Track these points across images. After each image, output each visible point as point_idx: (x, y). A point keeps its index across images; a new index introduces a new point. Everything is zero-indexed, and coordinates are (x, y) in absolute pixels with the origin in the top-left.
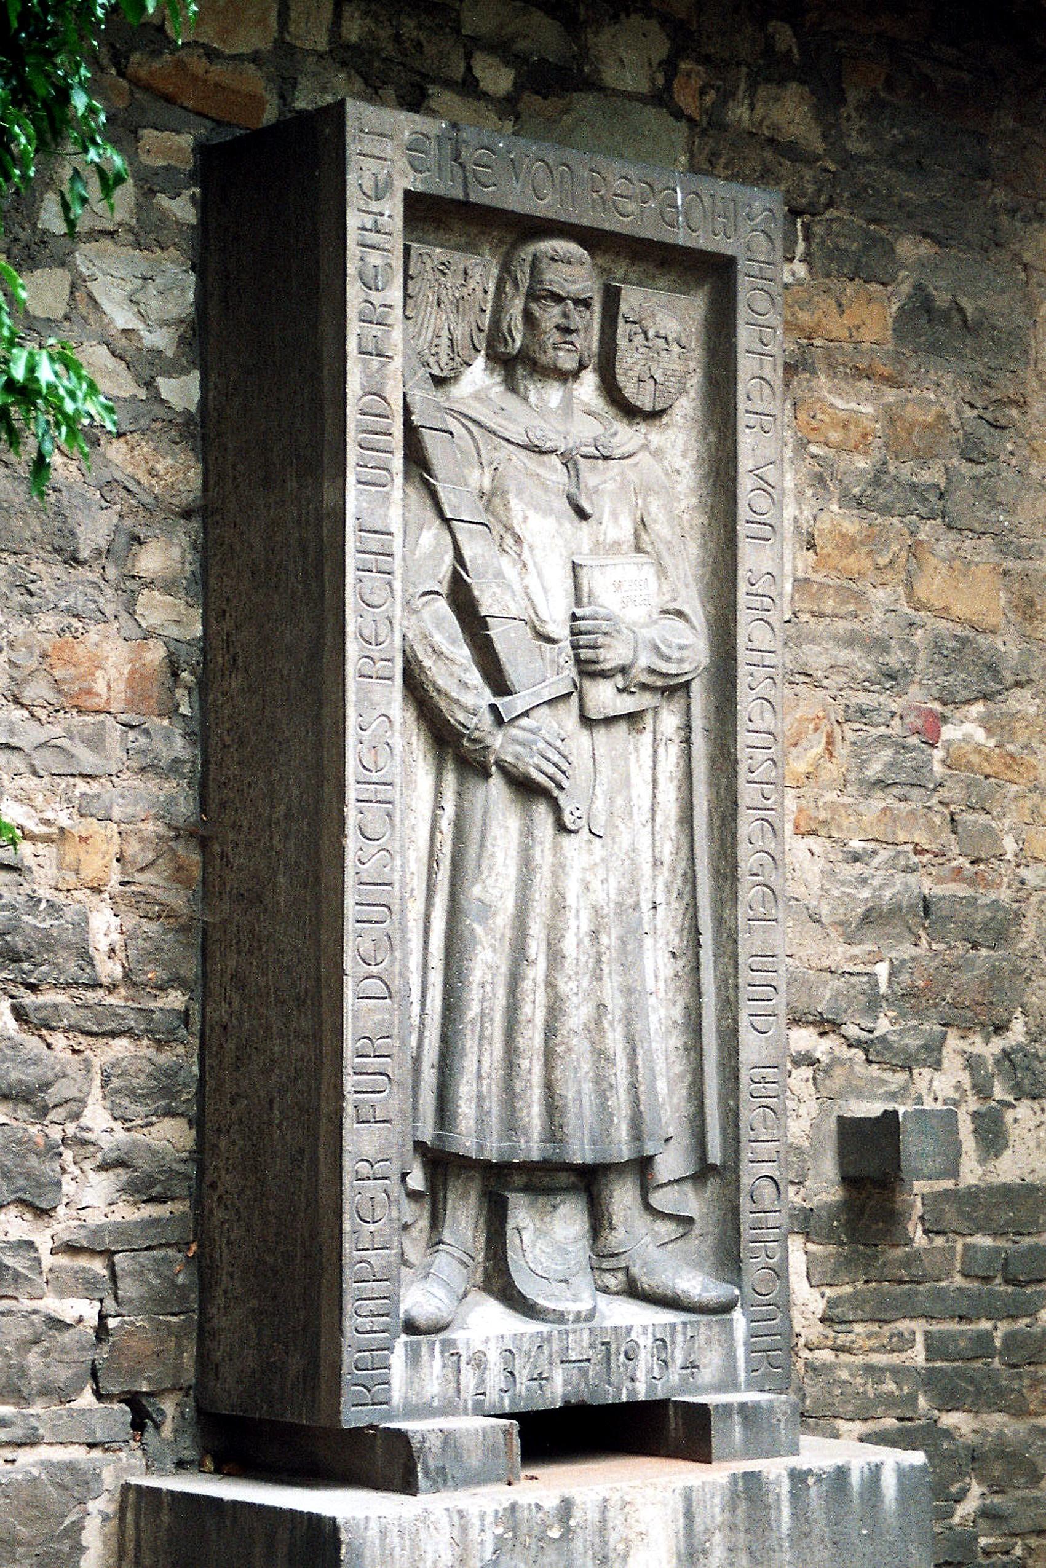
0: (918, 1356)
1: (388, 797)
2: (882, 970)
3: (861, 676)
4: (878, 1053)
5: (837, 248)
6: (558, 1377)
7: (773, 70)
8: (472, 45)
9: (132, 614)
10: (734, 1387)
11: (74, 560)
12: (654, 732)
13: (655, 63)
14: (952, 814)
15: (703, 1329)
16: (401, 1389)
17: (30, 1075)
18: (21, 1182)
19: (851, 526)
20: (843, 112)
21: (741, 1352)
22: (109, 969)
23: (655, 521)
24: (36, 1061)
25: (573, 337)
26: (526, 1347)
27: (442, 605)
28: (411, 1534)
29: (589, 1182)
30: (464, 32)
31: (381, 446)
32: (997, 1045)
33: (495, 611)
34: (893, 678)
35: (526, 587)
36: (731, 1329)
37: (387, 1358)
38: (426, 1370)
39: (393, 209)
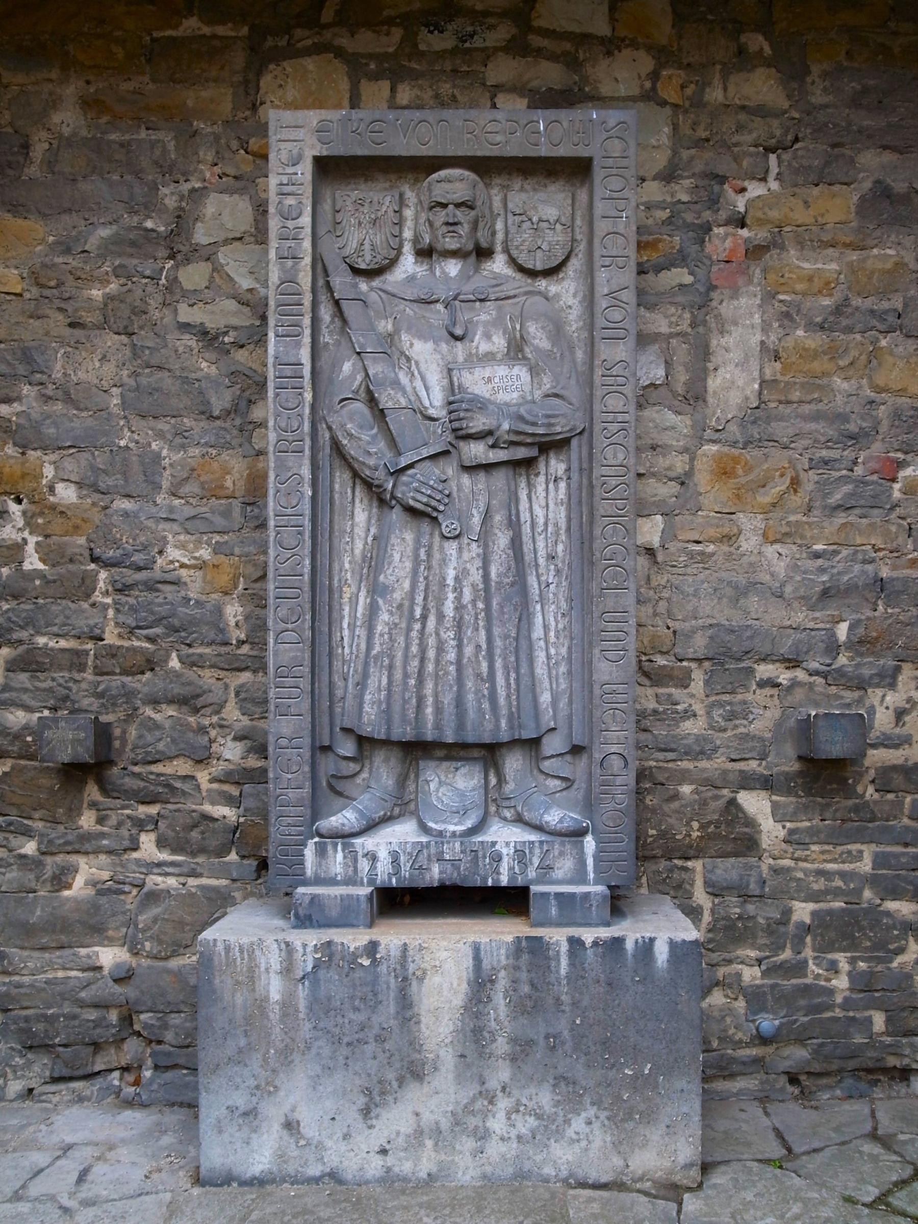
0: (866, 866)
1: (300, 523)
3: (823, 439)
4: (835, 679)
5: (802, 166)
6: (436, 870)
7: (744, 60)
9: (250, 443)
10: (583, 881)
12: (547, 474)
13: (643, 76)
14: (909, 524)
15: (557, 846)
18: (182, 746)
19: (815, 341)
20: (809, 80)
21: (590, 862)
23: (534, 338)
24: (190, 684)
25: (458, 228)
26: (409, 850)
27: (359, 407)
29: (489, 753)
30: (488, 83)
31: (294, 312)
33: (390, 404)
34: (855, 439)
35: (414, 388)
36: (582, 847)
37: (302, 850)
38: (331, 859)
39: (305, 171)
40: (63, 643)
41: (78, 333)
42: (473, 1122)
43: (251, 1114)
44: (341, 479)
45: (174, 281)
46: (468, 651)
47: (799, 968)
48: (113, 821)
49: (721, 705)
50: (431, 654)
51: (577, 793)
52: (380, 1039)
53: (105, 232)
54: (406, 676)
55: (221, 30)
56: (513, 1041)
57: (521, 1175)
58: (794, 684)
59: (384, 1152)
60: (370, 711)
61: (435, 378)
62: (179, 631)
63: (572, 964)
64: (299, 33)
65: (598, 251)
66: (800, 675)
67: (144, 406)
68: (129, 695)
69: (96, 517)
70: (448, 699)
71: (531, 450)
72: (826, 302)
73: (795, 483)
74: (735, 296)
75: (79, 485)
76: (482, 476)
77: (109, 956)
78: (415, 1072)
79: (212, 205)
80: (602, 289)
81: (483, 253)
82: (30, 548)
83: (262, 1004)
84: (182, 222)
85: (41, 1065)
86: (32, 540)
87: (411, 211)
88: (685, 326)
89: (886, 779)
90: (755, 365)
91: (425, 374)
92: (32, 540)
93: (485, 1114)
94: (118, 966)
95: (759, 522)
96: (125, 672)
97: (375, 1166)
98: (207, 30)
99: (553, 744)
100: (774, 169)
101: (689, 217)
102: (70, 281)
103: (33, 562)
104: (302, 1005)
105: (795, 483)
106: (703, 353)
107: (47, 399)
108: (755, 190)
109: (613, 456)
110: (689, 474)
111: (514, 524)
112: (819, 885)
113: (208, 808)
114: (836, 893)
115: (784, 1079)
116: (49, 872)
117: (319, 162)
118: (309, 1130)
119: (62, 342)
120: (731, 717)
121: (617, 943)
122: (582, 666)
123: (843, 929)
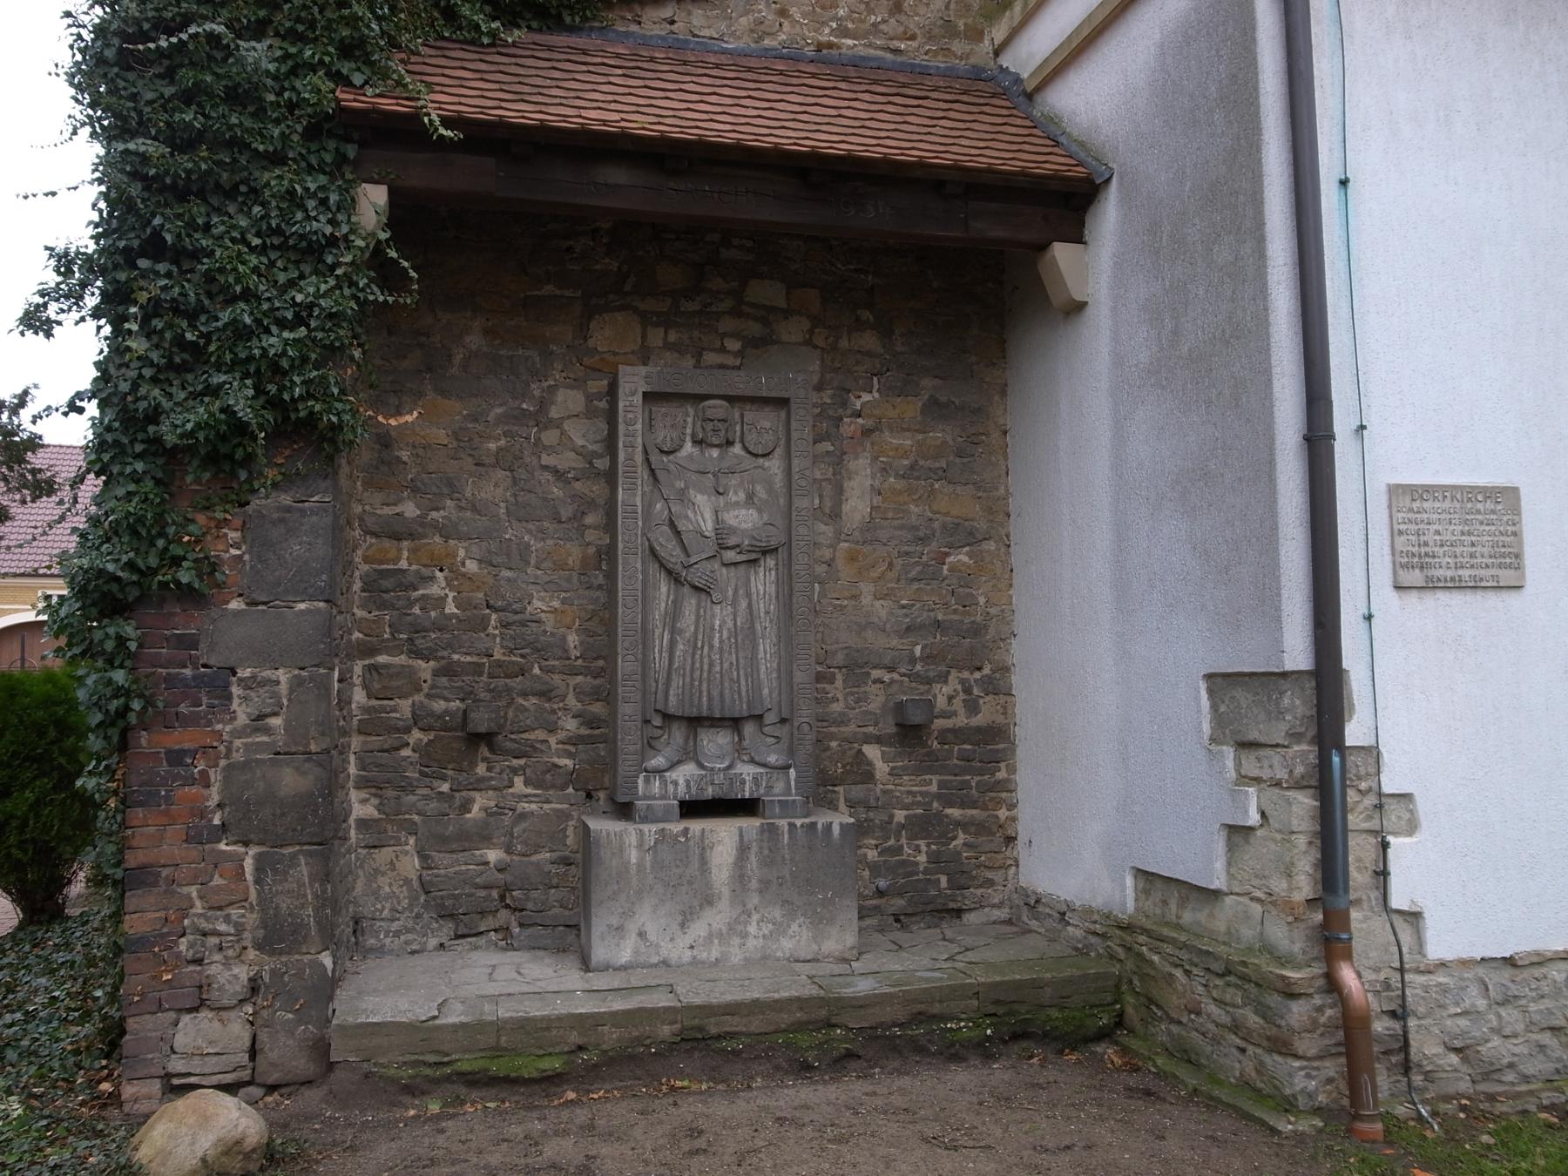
0: (934, 788)
2: (918, 648)
8: (723, 336)
11: (560, 522)
16: (647, 790)
17: (544, 688)
19: (900, 485)
22: (575, 653)
27: (666, 529)
28: (620, 835)
29: (735, 723)
32: (977, 675)
34: (923, 540)
39: (638, 399)
40: (469, 659)
41: (481, 469)
42: (740, 928)
43: (620, 928)
44: (653, 567)
45: (538, 439)
46: (726, 665)
47: (899, 850)
48: (498, 769)
49: (852, 694)
50: (706, 667)
51: (784, 744)
52: (690, 883)
53: (499, 410)
54: (692, 679)
55: (567, 293)
56: (760, 881)
57: (765, 958)
58: (892, 681)
59: (692, 947)
60: (672, 700)
61: (708, 515)
62: (540, 651)
63: (790, 838)
64: (611, 297)
65: (793, 448)
66: (895, 676)
67: (518, 513)
68: (509, 690)
69: (491, 581)
70: (715, 693)
71: (758, 554)
72: (906, 462)
73: (891, 565)
74: (856, 458)
75: (480, 561)
76: (732, 569)
77: (493, 855)
78: (709, 901)
79: (560, 395)
80: (795, 469)
81: (730, 443)
82: (450, 599)
83: (626, 865)
84: (543, 405)
85: (448, 928)
86: (451, 595)
87: (688, 417)
88: (829, 475)
89: (943, 736)
90: (868, 498)
91: (702, 514)
92: (451, 595)
93: (746, 923)
94: (500, 861)
95: (871, 587)
96: (507, 676)
97: (687, 955)
98: (558, 292)
99: (770, 718)
100: (876, 386)
101: (831, 412)
102: (477, 439)
103: (451, 608)
104: (648, 865)
105: (891, 565)
106: (840, 490)
107: (461, 508)
108: (866, 397)
109: (801, 560)
110: (833, 559)
111: (748, 595)
112: (909, 800)
113: (556, 760)
114: (918, 804)
115: (891, 919)
116: (457, 802)
117: (647, 396)
118: (652, 937)
119: (471, 475)
120: (858, 701)
121: (814, 825)
122: (785, 673)
123: (924, 825)
